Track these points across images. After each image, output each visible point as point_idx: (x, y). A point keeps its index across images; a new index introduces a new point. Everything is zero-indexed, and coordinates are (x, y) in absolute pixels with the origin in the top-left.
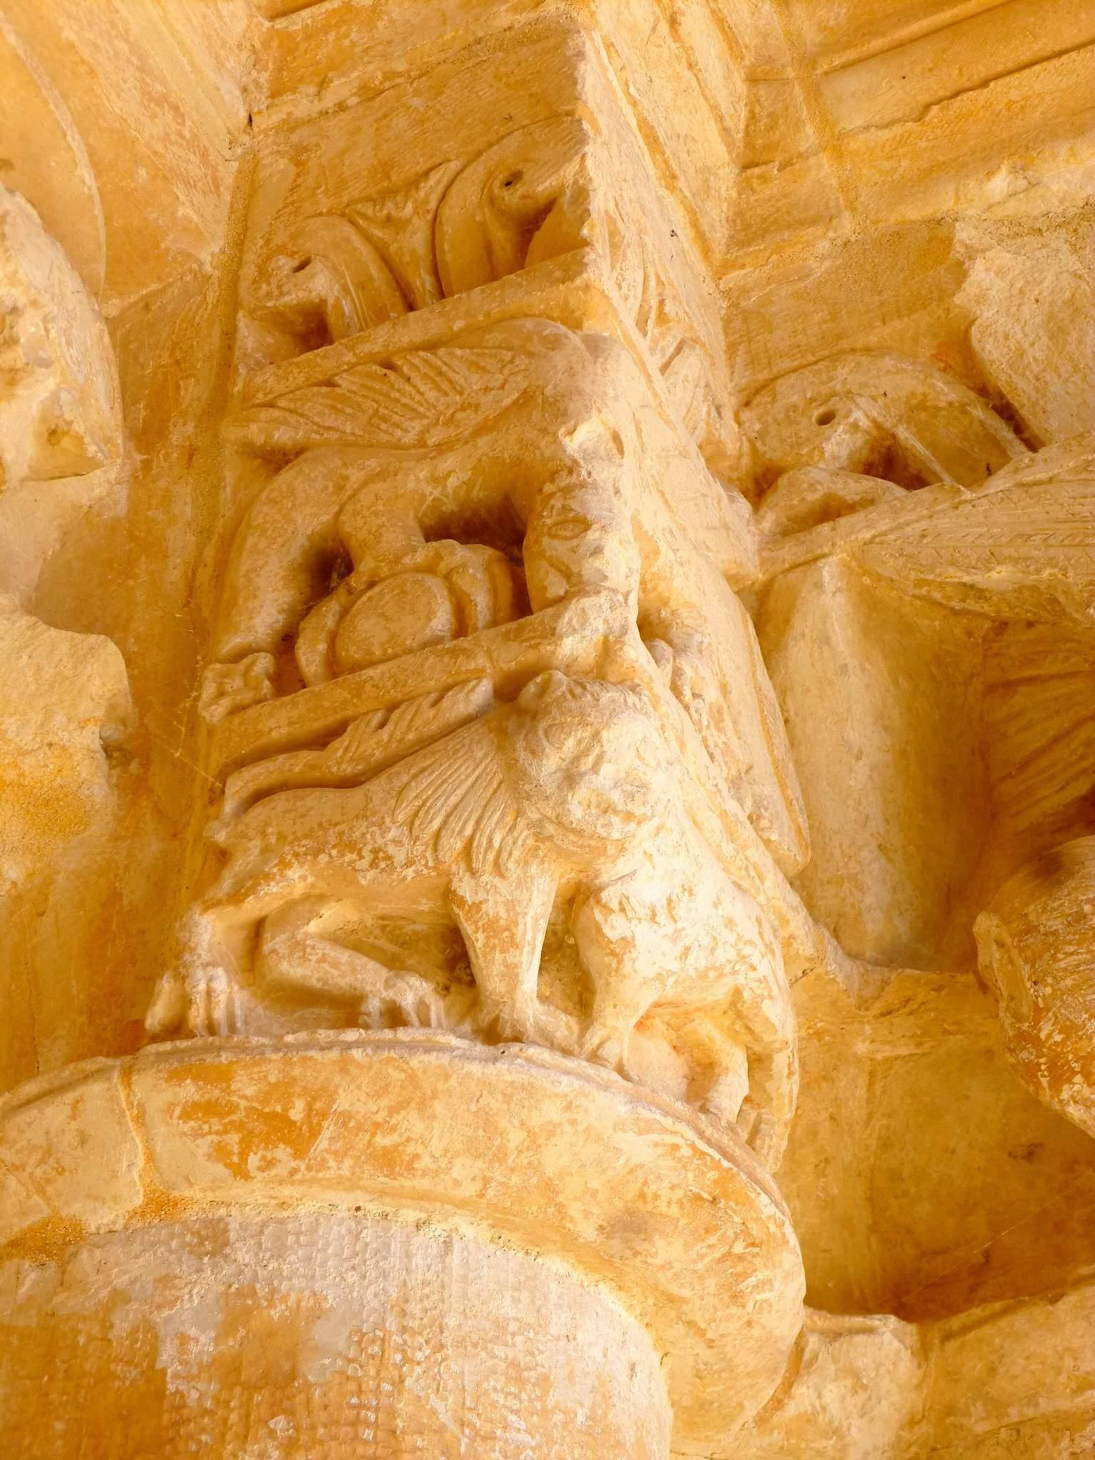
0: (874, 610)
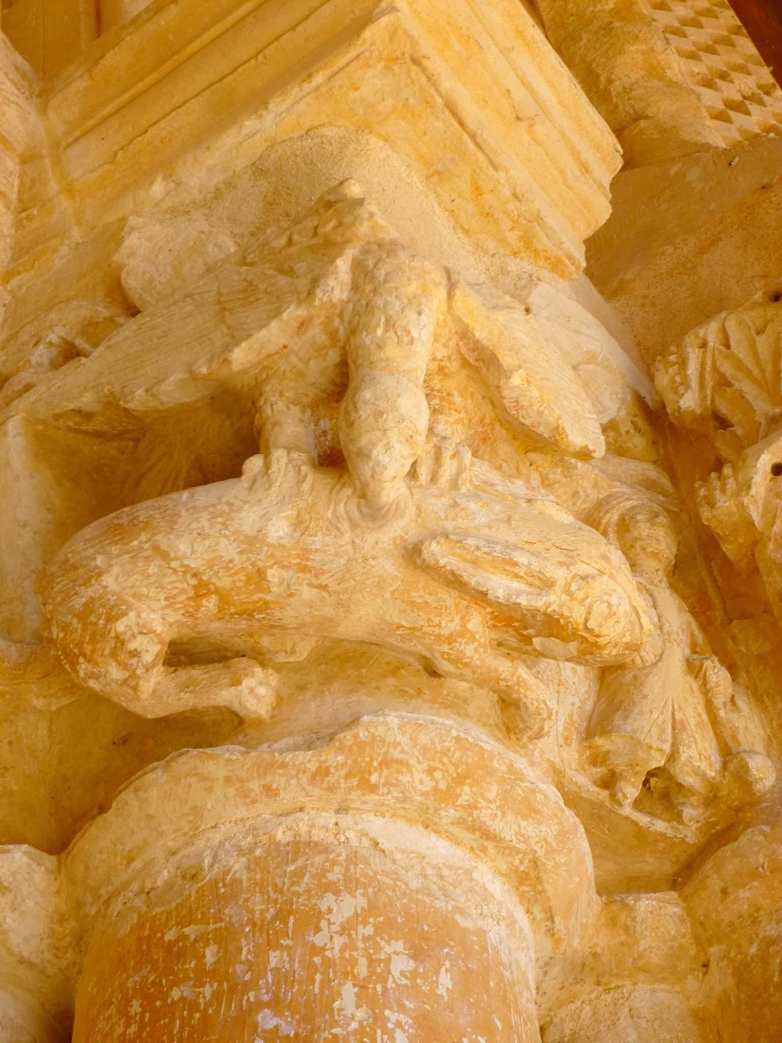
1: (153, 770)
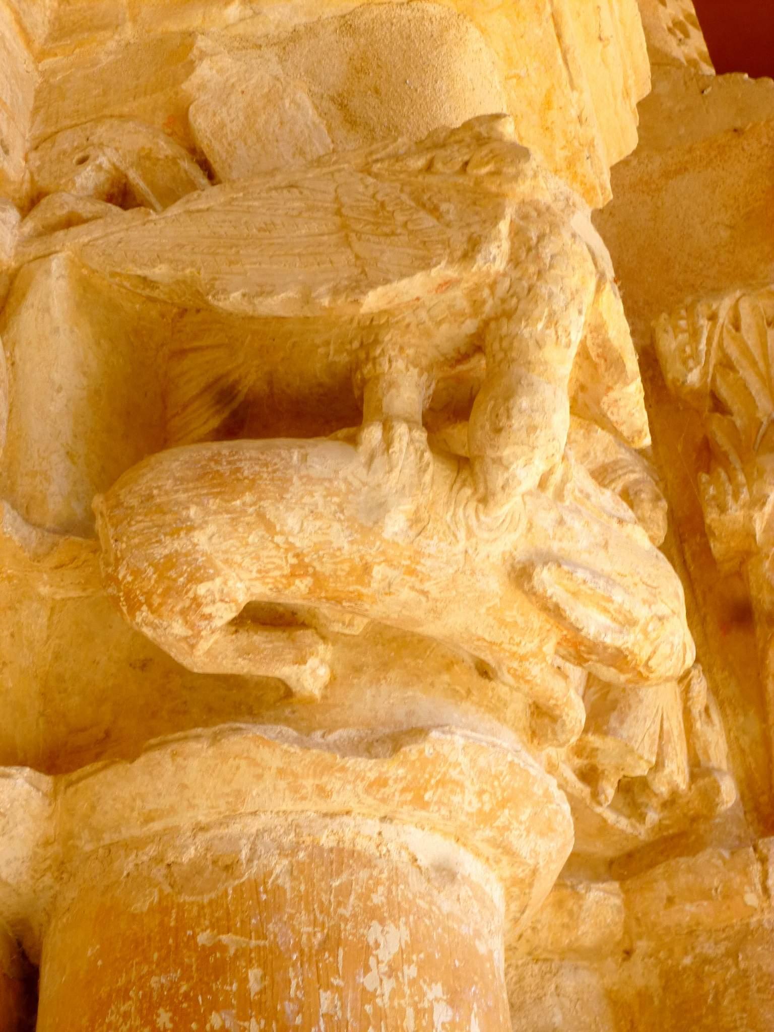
0: (87, 291)
1: (198, 737)
